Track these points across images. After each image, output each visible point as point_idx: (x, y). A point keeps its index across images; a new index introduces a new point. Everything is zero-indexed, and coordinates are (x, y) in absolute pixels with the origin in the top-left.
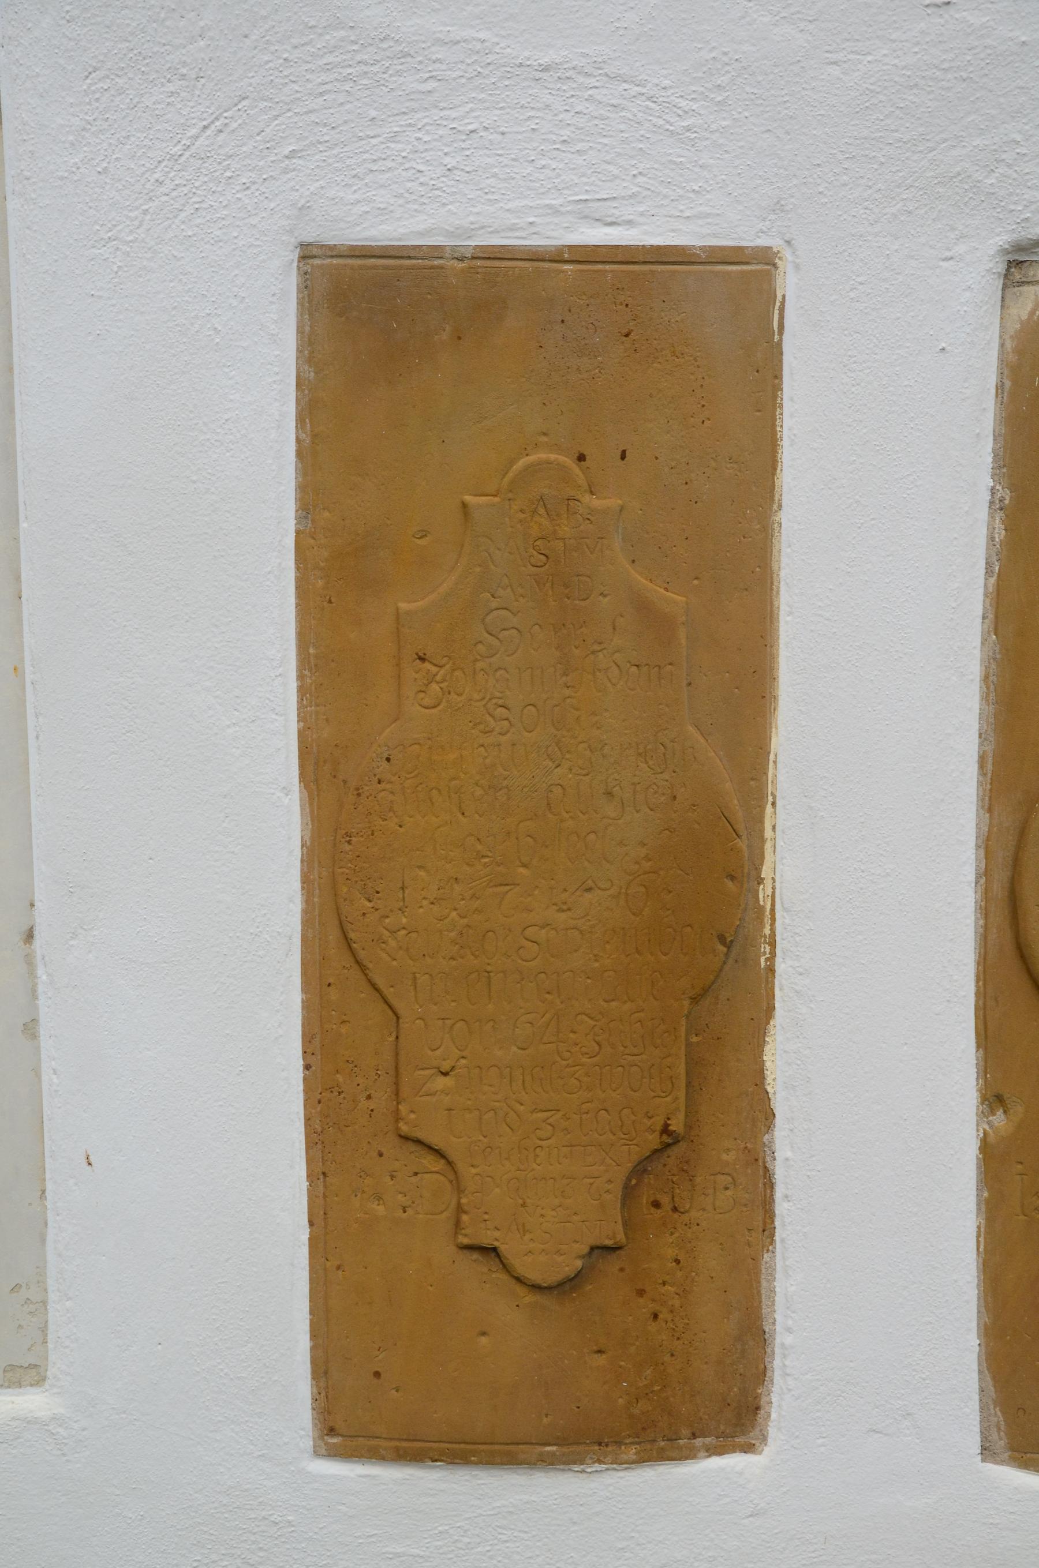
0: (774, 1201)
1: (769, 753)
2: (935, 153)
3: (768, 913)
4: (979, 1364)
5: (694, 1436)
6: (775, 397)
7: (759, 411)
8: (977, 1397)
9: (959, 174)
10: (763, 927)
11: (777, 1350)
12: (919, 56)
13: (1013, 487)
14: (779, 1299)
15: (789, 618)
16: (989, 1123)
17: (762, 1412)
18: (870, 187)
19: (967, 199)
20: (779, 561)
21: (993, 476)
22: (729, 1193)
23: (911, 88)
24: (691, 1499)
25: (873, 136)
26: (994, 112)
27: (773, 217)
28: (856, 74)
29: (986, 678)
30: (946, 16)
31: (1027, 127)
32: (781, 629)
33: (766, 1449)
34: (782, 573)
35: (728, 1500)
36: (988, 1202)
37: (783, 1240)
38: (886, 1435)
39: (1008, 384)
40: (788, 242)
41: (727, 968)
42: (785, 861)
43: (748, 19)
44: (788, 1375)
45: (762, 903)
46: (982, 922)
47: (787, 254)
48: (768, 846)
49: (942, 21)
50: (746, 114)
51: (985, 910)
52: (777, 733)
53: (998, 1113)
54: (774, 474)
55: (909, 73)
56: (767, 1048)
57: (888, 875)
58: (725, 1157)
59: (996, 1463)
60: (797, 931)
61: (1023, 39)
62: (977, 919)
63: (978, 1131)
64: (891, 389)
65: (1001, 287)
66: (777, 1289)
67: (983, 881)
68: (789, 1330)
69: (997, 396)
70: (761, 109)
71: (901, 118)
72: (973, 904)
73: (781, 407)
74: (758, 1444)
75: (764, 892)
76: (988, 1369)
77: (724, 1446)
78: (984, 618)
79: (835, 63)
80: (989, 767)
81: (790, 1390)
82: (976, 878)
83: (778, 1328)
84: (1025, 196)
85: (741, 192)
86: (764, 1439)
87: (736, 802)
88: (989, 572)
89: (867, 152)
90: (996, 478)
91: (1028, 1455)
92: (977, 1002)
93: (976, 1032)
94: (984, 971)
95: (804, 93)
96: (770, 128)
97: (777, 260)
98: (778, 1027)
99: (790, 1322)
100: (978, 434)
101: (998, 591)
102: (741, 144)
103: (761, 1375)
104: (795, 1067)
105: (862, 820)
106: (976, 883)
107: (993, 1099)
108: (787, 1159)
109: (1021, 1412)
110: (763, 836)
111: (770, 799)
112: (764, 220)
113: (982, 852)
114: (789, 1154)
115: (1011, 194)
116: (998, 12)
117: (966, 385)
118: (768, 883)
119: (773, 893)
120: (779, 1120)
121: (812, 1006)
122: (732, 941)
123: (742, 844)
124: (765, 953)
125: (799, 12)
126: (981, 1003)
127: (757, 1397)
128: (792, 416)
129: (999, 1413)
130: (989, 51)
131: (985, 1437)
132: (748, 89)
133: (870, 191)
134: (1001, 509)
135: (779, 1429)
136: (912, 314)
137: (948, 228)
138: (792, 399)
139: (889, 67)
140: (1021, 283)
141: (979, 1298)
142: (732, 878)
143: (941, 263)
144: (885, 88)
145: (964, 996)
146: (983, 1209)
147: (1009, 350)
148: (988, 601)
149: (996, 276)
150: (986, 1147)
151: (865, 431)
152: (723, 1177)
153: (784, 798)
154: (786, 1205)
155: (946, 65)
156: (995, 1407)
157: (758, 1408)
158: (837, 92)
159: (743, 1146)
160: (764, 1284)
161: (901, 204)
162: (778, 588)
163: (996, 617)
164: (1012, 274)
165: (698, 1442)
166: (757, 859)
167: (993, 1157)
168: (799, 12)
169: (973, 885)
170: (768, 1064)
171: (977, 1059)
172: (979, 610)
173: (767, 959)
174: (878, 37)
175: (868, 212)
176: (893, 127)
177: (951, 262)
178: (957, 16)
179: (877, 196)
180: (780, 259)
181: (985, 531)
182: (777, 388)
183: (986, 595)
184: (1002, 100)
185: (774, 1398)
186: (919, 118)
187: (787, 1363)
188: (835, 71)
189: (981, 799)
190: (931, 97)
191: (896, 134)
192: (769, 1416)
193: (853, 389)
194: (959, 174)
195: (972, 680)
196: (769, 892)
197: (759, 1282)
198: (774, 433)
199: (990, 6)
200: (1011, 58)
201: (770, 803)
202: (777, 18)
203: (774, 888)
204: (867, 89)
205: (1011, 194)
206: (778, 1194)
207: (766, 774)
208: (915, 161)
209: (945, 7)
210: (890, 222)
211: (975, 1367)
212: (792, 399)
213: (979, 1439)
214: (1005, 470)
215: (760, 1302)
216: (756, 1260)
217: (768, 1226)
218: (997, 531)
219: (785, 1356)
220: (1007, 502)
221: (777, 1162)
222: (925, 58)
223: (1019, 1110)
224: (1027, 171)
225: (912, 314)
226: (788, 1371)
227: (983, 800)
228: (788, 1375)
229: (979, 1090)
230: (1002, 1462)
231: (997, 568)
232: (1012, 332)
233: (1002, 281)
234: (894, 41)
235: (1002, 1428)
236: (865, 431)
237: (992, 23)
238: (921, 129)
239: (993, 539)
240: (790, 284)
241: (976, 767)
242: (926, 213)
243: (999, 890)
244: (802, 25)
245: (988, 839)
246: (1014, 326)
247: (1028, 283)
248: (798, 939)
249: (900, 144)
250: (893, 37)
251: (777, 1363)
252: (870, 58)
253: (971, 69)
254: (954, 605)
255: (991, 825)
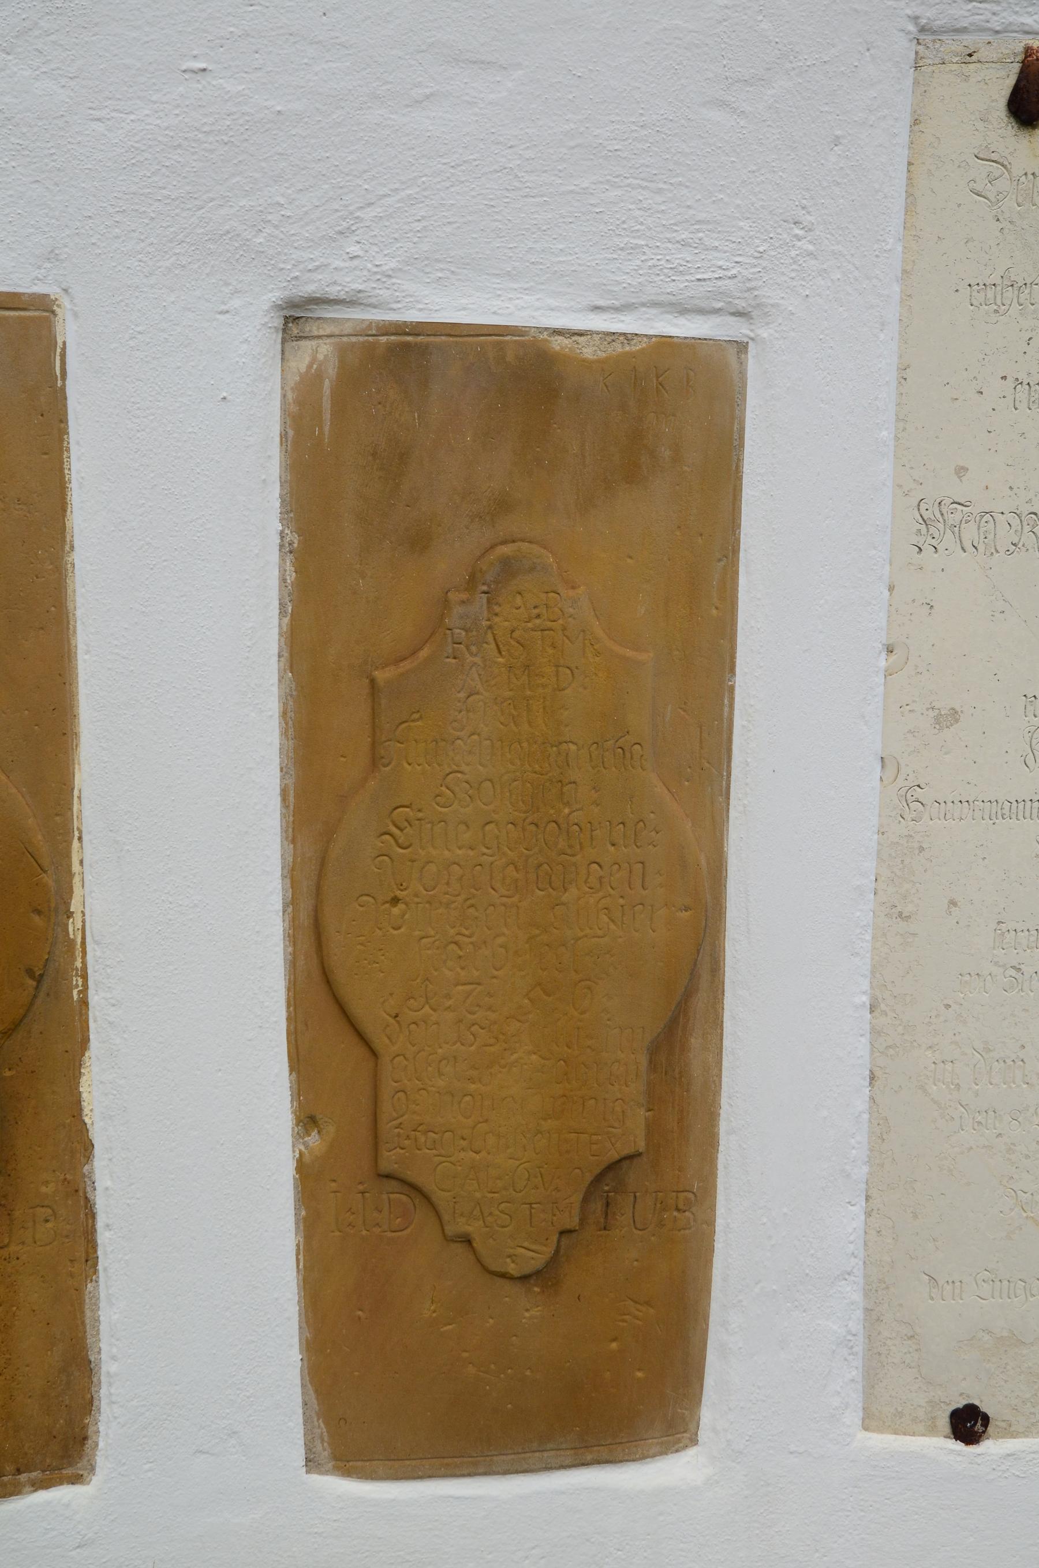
0: (96, 1231)
1: (73, 789)
2: (203, 211)
3: (78, 946)
4: (302, 1379)
5: (19, 1471)
6: (62, 440)
7: (46, 454)
8: (300, 1411)
9: (228, 232)
10: (75, 960)
11: (103, 1378)
12: (180, 118)
13: (300, 531)
14: (103, 1328)
15: (86, 657)
16: (304, 1144)
17: (90, 1442)
18: (143, 241)
19: (238, 256)
20: (74, 601)
21: (281, 521)
22: (49, 1225)
23: (176, 147)
24: (16, 1536)
25: (142, 192)
26: (257, 175)
27: (48, 265)
28: (120, 131)
29: (284, 714)
30: (204, 82)
31: (289, 191)
32: (79, 667)
33: (95, 1479)
34: (79, 613)
35: (55, 1533)
36: (305, 1219)
37: (105, 1270)
38: (213, 1455)
39: (291, 433)
40: (66, 290)
41: (39, 1001)
42: (93, 894)
43: (8, 72)
44: (114, 1403)
45: (72, 936)
46: (290, 949)
47: (65, 301)
48: (76, 880)
49: (200, 86)
50: (13, 164)
51: (292, 937)
52: (80, 769)
53: (313, 1134)
54: (64, 516)
55: (171, 134)
56: (84, 1080)
57: (196, 906)
58: (44, 1189)
59: (321, 1473)
60: (108, 963)
61: (279, 108)
62: (285, 946)
63: (294, 1152)
64: (175, 435)
65: (280, 341)
66: (102, 1318)
67: (290, 910)
68: (114, 1358)
69: (281, 445)
70: (29, 159)
71: (168, 176)
72: (281, 932)
73: (68, 450)
74: (86, 1474)
75: (73, 927)
76: (311, 1383)
77: (51, 1479)
78: (279, 657)
79: (98, 120)
80: (291, 799)
81: (115, 1418)
82: (284, 907)
83: (103, 1356)
84: (293, 256)
85: (13, 239)
86: (92, 1469)
87: (40, 837)
88: (282, 612)
89: (137, 207)
90: (285, 522)
91: (351, 1463)
92: (288, 1027)
93: (289, 1056)
94: (294, 998)
95: (69, 147)
96: (38, 179)
97: (55, 308)
98: (93, 1058)
99: (114, 1350)
100: (264, 480)
101: (292, 630)
102: (10, 192)
103: (88, 1405)
104: (112, 1097)
105: (168, 853)
106: (284, 912)
107: (307, 1120)
108: (107, 1189)
109: (342, 1422)
110: (70, 871)
111: (76, 834)
112: (39, 268)
113: (288, 881)
114: (109, 1183)
115: (279, 253)
116: (253, 81)
117: (249, 433)
118: (78, 917)
119: (84, 927)
120: (98, 1151)
121: (125, 1036)
122: (41, 976)
123: (48, 879)
124: (77, 986)
125: (58, 68)
126: (292, 1027)
127: (84, 1427)
128: (79, 459)
129: (322, 1425)
130: (247, 118)
131: (309, 1449)
132: (12, 139)
133: (142, 245)
134: (291, 552)
135: (106, 1457)
136: (192, 363)
137: (221, 283)
138: (78, 443)
139: (152, 127)
140: (299, 338)
141: (300, 1315)
142: (38, 912)
143: (218, 316)
144: (150, 146)
145: (276, 1022)
146: (302, 1228)
147: (291, 401)
148: (283, 640)
149: (273, 330)
150: (301, 1167)
151: (152, 475)
152: (43, 1210)
153: (90, 833)
154: (107, 1234)
155: (206, 129)
156: (318, 1420)
157: (85, 1438)
158: (103, 147)
159: (62, 1177)
160: (88, 1313)
161: (174, 258)
162: (75, 627)
163: (291, 655)
164: (291, 329)
165: (23, 1477)
166: (65, 892)
167: (309, 1177)
168: (58, 68)
169: (281, 914)
170: (84, 1095)
171: (291, 1082)
172: (275, 650)
173: (80, 992)
174: (139, 97)
175: (142, 264)
176: (160, 184)
177: (227, 316)
178: (214, 83)
179: (151, 249)
180: (59, 306)
181: (276, 573)
182: (62, 431)
183: (280, 634)
184: (263, 164)
185: (102, 1428)
186: (185, 177)
187: (113, 1391)
188: (99, 127)
189: (284, 831)
190: (195, 157)
191: (164, 191)
192: (97, 1445)
193: (139, 435)
194: (228, 232)
195: (271, 716)
196: (79, 925)
197: (83, 1312)
198: (62, 476)
199: (245, 75)
200: (269, 126)
201: (76, 838)
202: (37, 72)
203: (84, 922)
204: (132, 146)
205: (279, 253)
206: (100, 1224)
207: (71, 809)
208: (184, 218)
209: (202, 73)
210: (164, 275)
211: (298, 1381)
212: (78, 443)
213: (303, 1452)
214: (292, 515)
215: (85, 1332)
216: (79, 1291)
217: (91, 1256)
218: (288, 573)
219: (110, 1384)
220: (295, 545)
221: (97, 1192)
222: (186, 120)
223: (331, 1129)
224: (293, 232)
225: (192, 363)
226: (114, 1399)
227: (286, 832)
228: (114, 1403)
229: (294, 1112)
230: (326, 1473)
231: (290, 609)
232: (291, 383)
233: (280, 335)
234: (155, 102)
235: (326, 1439)
236: (152, 475)
237: (247, 92)
238: (188, 188)
239: (284, 580)
240: (70, 331)
241: (279, 799)
242: (199, 268)
243: (305, 918)
244: (63, 81)
245: (293, 870)
246: (294, 379)
247: (306, 338)
248: (109, 971)
249: (169, 201)
250: (154, 98)
251: (103, 1392)
252: (132, 117)
253: (231, 133)
254: (249, 644)
255: (295, 855)
